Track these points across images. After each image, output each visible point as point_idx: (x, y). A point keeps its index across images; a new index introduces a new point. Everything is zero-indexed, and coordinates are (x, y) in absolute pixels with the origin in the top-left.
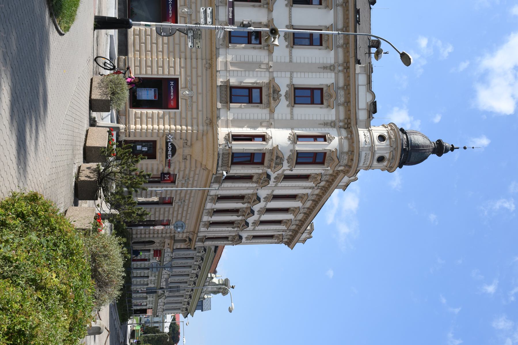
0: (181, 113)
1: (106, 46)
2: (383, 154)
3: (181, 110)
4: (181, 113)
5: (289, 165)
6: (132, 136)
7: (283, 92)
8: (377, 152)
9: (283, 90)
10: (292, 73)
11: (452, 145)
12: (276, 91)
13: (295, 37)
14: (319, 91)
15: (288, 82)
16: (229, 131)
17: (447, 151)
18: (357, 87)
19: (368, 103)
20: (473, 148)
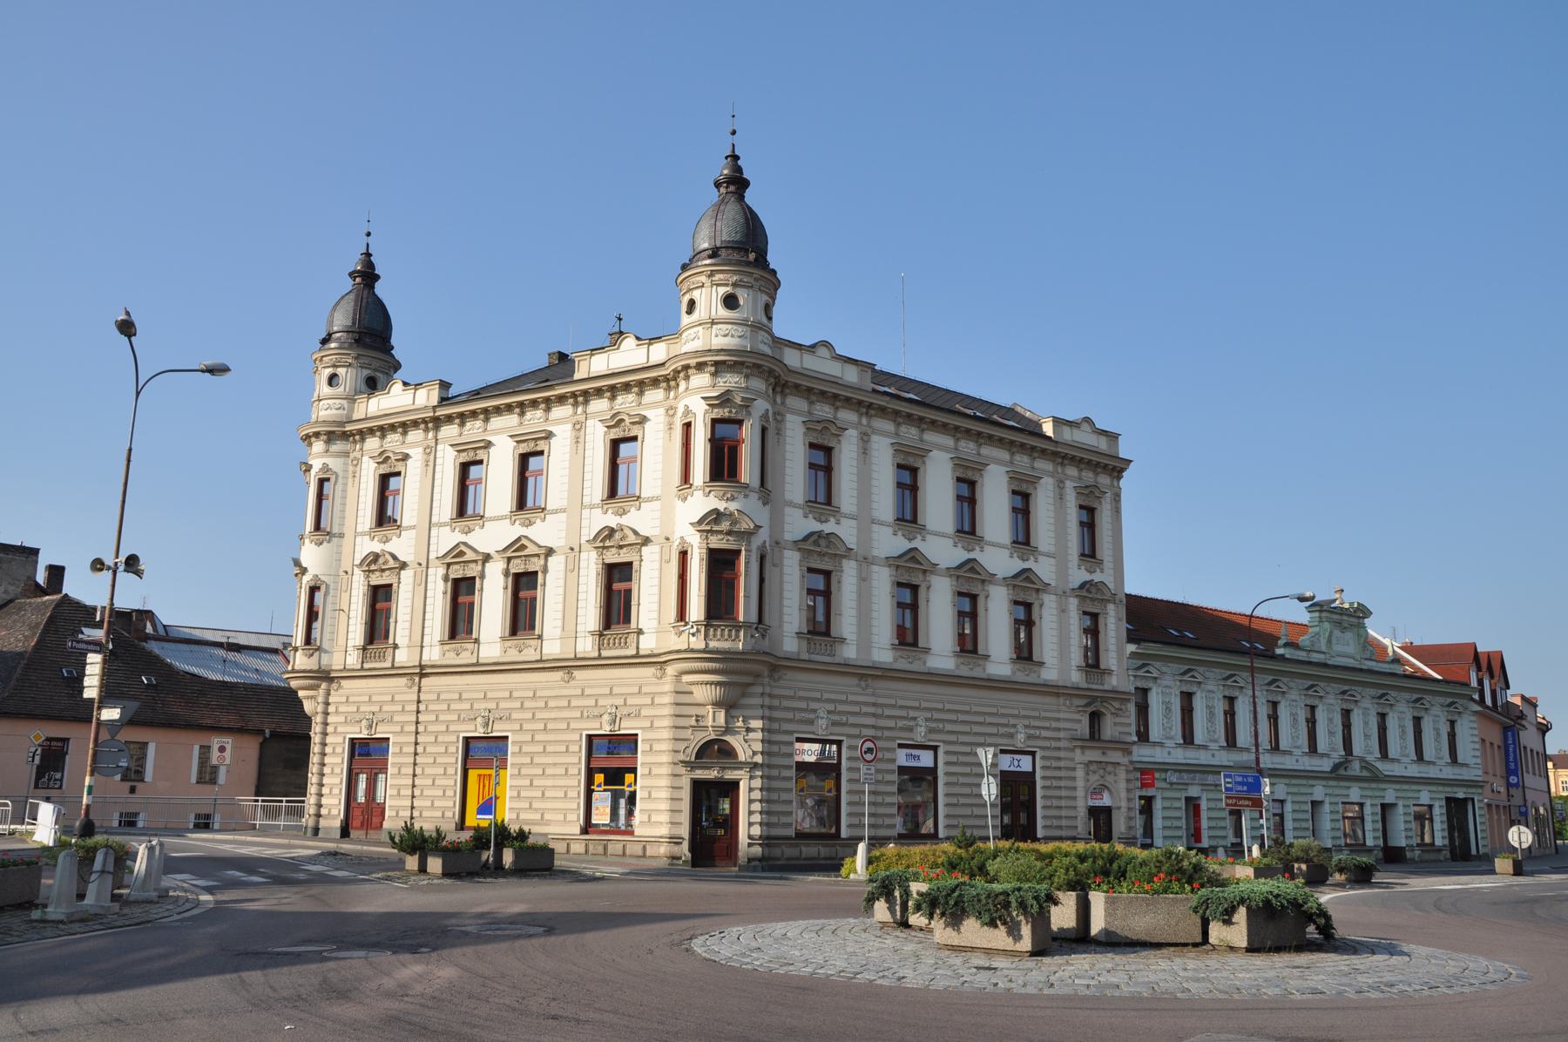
0: (1042, 748)
1: (373, 842)
2: (719, 298)
3: (1039, 747)
4: (1042, 748)
5: (1098, 570)
6: (677, 794)
7: (816, 526)
8: (759, 318)
9: (813, 525)
10: (873, 522)
11: (726, 158)
12: (814, 537)
13: (814, 500)
14: (718, 426)
15: (799, 513)
16: (1075, 668)
17: (739, 170)
18: (805, 372)
19: (833, 357)
20: (734, 116)
